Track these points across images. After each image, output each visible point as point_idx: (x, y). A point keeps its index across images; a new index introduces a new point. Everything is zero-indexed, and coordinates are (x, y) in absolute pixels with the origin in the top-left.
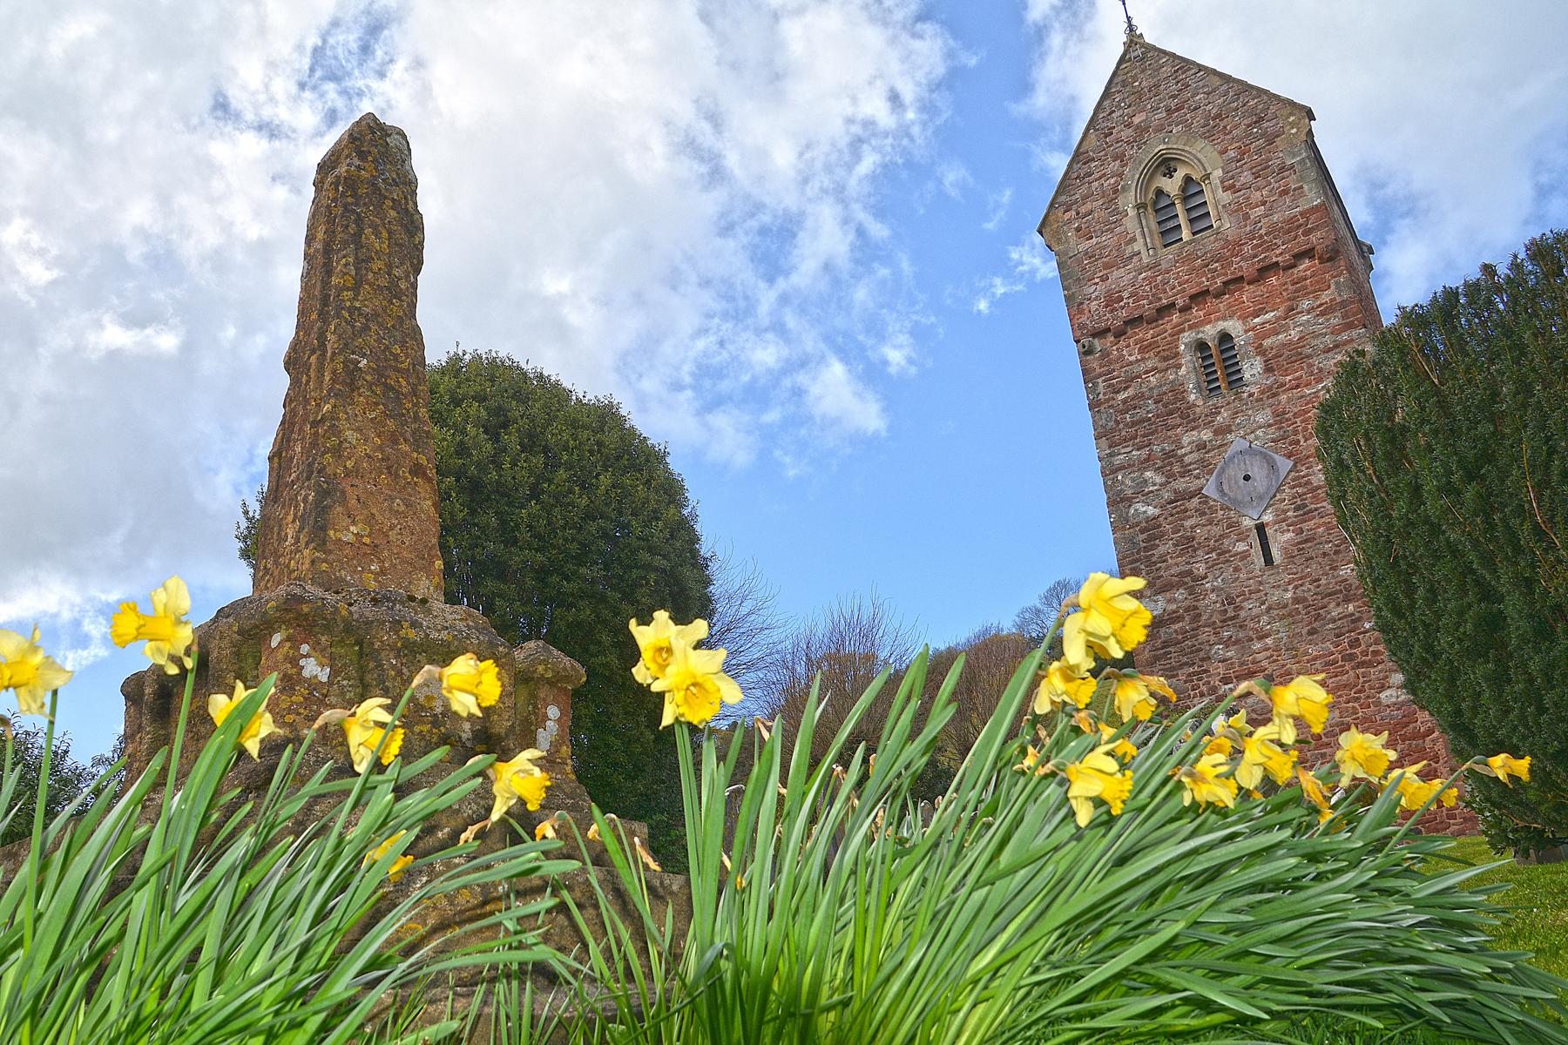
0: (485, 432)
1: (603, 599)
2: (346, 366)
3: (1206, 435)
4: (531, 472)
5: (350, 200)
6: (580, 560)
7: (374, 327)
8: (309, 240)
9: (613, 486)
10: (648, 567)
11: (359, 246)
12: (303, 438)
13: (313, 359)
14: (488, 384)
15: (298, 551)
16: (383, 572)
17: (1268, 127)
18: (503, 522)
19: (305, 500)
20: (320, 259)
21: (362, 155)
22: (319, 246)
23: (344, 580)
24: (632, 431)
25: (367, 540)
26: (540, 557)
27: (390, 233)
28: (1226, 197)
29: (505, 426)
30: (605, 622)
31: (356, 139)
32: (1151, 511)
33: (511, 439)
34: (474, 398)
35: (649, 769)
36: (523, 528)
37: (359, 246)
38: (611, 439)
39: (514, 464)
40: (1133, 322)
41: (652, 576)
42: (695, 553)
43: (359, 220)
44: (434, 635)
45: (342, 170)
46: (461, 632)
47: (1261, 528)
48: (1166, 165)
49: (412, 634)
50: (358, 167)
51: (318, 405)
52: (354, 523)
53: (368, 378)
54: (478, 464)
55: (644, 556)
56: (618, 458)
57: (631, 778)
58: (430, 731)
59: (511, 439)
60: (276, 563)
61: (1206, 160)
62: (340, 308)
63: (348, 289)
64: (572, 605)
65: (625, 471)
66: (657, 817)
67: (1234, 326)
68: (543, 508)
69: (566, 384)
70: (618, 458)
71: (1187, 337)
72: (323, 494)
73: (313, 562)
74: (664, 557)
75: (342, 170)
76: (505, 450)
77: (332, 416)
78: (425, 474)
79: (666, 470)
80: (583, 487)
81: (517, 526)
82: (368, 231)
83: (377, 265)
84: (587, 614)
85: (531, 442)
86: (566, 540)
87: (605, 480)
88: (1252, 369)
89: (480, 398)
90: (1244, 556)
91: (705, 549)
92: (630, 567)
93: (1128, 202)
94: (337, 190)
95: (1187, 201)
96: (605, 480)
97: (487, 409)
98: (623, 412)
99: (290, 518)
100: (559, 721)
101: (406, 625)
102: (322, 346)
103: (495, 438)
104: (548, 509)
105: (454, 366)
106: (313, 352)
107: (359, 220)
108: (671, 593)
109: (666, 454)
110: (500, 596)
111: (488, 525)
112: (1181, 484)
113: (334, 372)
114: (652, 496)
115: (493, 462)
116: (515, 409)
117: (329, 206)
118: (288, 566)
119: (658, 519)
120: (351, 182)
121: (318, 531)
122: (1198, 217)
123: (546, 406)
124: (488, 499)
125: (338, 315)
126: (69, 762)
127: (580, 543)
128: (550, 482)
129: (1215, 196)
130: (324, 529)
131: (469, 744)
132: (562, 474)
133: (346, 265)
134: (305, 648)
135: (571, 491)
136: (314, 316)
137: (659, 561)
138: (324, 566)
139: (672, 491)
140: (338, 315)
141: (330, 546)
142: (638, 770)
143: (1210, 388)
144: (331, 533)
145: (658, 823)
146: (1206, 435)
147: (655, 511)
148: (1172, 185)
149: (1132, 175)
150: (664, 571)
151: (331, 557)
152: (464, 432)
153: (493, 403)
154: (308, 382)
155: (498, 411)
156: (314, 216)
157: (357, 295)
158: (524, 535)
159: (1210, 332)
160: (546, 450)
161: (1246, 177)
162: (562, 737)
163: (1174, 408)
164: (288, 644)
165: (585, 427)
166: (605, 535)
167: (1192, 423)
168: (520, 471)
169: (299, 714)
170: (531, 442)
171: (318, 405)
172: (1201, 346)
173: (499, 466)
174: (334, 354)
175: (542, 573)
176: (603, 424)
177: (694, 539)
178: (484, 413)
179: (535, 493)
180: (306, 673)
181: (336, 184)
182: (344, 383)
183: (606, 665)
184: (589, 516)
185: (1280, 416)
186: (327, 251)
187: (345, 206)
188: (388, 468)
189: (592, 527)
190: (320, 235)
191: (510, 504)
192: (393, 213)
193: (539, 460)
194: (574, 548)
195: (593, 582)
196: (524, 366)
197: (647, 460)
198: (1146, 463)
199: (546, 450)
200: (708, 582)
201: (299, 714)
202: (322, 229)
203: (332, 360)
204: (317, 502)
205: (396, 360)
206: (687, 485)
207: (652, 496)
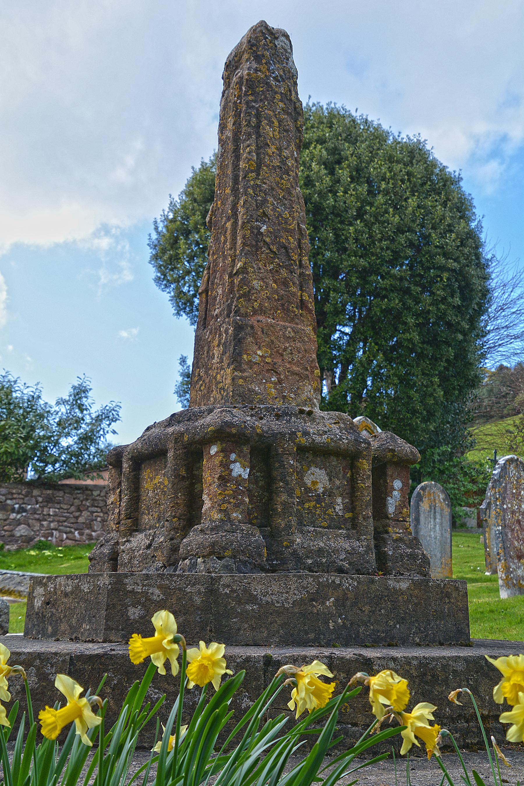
0: (326, 168)
1: (407, 291)
2: (252, 232)
4: (358, 198)
5: (250, 98)
6: (392, 263)
7: (270, 199)
8: (222, 128)
9: (419, 207)
10: (442, 268)
11: (258, 135)
12: (223, 284)
13: (229, 225)
14: (327, 130)
15: (222, 369)
16: (280, 382)
18: (337, 236)
19: (226, 331)
20: (230, 146)
21: (258, 58)
22: (230, 134)
23: (254, 391)
24: (434, 164)
25: (268, 360)
26: (362, 262)
27: (280, 122)
29: (339, 162)
30: (409, 309)
31: (252, 45)
33: (343, 174)
34: (317, 141)
35: (438, 414)
36: (351, 241)
37: (258, 135)
38: (418, 169)
39: (345, 192)
41: (445, 275)
42: (478, 256)
43: (258, 116)
44: (318, 439)
45: (243, 72)
46: (335, 435)
49: (303, 441)
50: (256, 70)
51: (233, 261)
52: (259, 348)
53: (268, 240)
54: (320, 193)
55: (441, 260)
56: (423, 184)
57: (425, 420)
58: (315, 507)
59: (343, 174)
60: (206, 373)
62: (246, 188)
63: (252, 172)
64: (385, 297)
65: (428, 194)
66: (444, 448)
68: (366, 225)
69: (385, 127)
70: (423, 184)
72: (239, 328)
73: (233, 379)
74: (455, 260)
75: (243, 72)
76: (338, 181)
77: (244, 270)
78: (307, 307)
79: (460, 188)
80: (395, 208)
81: (346, 238)
82: (264, 122)
83: (272, 149)
84: (396, 303)
85: (358, 174)
86: (382, 249)
87: (413, 202)
89: (321, 141)
91: (487, 252)
92: (429, 269)
94: (241, 89)
96: (413, 202)
97: (326, 149)
98: (428, 147)
99: (216, 342)
100: (401, 490)
101: (299, 434)
102: (235, 214)
103: (332, 172)
104: (369, 225)
106: (228, 219)
107: (258, 116)
108: (459, 287)
109: (460, 179)
110: (334, 291)
111: (327, 239)
113: (244, 237)
114: (448, 214)
115: (330, 191)
116: (347, 150)
117: (235, 103)
118: (215, 378)
119: (451, 231)
120: (251, 84)
121: (236, 361)
123: (369, 146)
124: (327, 218)
125: (246, 193)
126: (41, 402)
127: (392, 251)
128: (371, 204)
130: (240, 355)
131: (340, 513)
132: (380, 199)
133: (249, 153)
134: (233, 456)
135: (386, 212)
136: (228, 191)
137: (452, 264)
138: (241, 381)
139: (462, 208)
140: (246, 193)
141: (245, 367)
142: (430, 416)
144: (245, 357)
145: (443, 452)
147: (449, 225)
150: (454, 271)
151: (246, 374)
152: (309, 168)
153: (330, 145)
154: (225, 242)
155: (334, 151)
156: (225, 108)
157: (258, 174)
158: (352, 245)
160: (369, 182)
162: (404, 502)
164: (222, 454)
165: (398, 162)
166: (411, 245)
168: (350, 197)
169: (230, 503)
170: (358, 174)
171: (233, 261)
173: (335, 193)
174: (244, 223)
175: (364, 274)
176: (412, 158)
177: (478, 245)
178: (324, 153)
179: (360, 215)
180: (234, 474)
181: (240, 83)
182: (251, 245)
183: (410, 340)
184: (400, 230)
186: (236, 140)
187: (247, 103)
188: (283, 305)
189: (402, 239)
190: (230, 126)
191: (342, 222)
192: (281, 105)
193: (364, 189)
194: (388, 255)
195: (401, 279)
196: (354, 114)
197: (444, 185)
199: (369, 182)
200: (486, 278)
201: (230, 503)
202: (230, 122)
203: (242, 228)
204: (236, 335)
205: (286, 223)
206: (475, 203)
207: (448, 214)
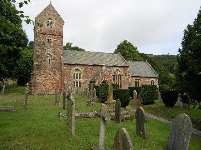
3: (46, 48)
17: (61, 22)
28: (55, 26)
32: (39, 54)
40: (42, 34)
47: (49, 59)
48: (50, 19)
61: (54, 21)
67: (52, 39)
71: (47, 38)
88: (52, 44)
90: (47, 61)
93: (45, 21)
95: (25, 1)
105: (194, 23)
112: (43, 52)
122: (51, 26)
129: (54, 25)
143: (48, 43)
146: (46, 48)
148: (50, 21)
149: (47, 18)
159: (49, 38)
161: (57, 25)
163: (44, 44)
167: (45, 46)
172: (48, 39)
185: (54, 50)
198: (39, 49)
